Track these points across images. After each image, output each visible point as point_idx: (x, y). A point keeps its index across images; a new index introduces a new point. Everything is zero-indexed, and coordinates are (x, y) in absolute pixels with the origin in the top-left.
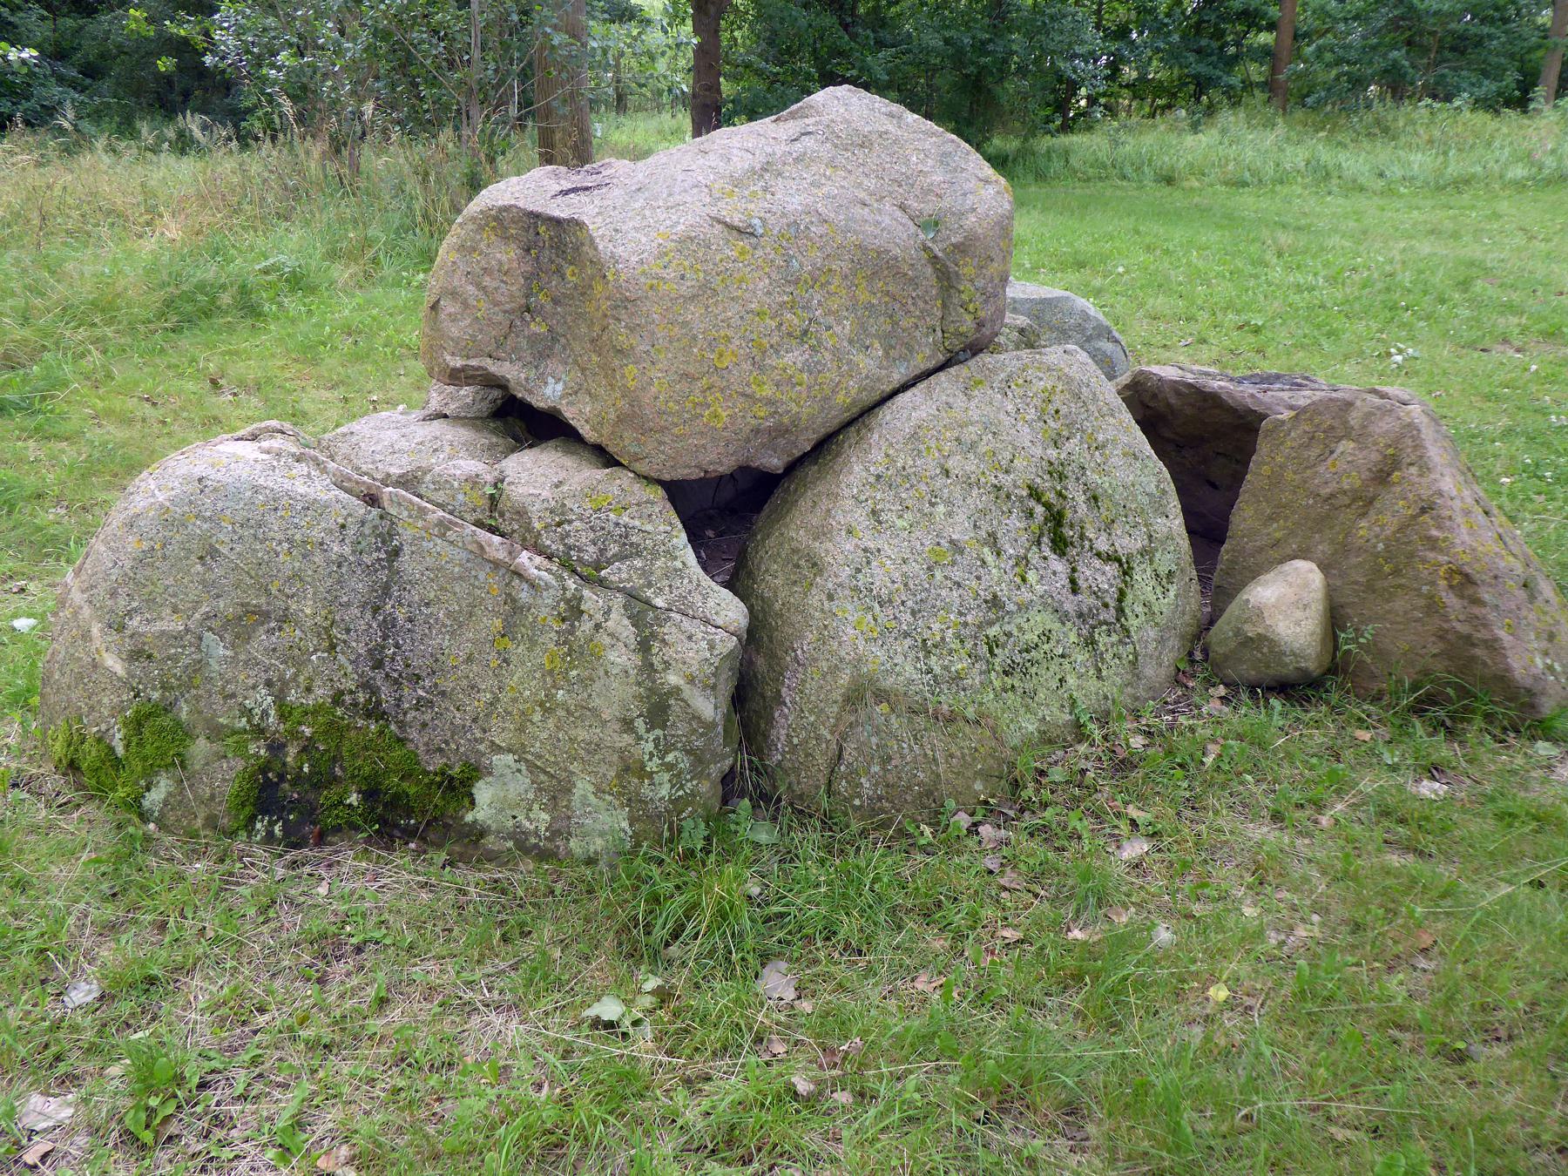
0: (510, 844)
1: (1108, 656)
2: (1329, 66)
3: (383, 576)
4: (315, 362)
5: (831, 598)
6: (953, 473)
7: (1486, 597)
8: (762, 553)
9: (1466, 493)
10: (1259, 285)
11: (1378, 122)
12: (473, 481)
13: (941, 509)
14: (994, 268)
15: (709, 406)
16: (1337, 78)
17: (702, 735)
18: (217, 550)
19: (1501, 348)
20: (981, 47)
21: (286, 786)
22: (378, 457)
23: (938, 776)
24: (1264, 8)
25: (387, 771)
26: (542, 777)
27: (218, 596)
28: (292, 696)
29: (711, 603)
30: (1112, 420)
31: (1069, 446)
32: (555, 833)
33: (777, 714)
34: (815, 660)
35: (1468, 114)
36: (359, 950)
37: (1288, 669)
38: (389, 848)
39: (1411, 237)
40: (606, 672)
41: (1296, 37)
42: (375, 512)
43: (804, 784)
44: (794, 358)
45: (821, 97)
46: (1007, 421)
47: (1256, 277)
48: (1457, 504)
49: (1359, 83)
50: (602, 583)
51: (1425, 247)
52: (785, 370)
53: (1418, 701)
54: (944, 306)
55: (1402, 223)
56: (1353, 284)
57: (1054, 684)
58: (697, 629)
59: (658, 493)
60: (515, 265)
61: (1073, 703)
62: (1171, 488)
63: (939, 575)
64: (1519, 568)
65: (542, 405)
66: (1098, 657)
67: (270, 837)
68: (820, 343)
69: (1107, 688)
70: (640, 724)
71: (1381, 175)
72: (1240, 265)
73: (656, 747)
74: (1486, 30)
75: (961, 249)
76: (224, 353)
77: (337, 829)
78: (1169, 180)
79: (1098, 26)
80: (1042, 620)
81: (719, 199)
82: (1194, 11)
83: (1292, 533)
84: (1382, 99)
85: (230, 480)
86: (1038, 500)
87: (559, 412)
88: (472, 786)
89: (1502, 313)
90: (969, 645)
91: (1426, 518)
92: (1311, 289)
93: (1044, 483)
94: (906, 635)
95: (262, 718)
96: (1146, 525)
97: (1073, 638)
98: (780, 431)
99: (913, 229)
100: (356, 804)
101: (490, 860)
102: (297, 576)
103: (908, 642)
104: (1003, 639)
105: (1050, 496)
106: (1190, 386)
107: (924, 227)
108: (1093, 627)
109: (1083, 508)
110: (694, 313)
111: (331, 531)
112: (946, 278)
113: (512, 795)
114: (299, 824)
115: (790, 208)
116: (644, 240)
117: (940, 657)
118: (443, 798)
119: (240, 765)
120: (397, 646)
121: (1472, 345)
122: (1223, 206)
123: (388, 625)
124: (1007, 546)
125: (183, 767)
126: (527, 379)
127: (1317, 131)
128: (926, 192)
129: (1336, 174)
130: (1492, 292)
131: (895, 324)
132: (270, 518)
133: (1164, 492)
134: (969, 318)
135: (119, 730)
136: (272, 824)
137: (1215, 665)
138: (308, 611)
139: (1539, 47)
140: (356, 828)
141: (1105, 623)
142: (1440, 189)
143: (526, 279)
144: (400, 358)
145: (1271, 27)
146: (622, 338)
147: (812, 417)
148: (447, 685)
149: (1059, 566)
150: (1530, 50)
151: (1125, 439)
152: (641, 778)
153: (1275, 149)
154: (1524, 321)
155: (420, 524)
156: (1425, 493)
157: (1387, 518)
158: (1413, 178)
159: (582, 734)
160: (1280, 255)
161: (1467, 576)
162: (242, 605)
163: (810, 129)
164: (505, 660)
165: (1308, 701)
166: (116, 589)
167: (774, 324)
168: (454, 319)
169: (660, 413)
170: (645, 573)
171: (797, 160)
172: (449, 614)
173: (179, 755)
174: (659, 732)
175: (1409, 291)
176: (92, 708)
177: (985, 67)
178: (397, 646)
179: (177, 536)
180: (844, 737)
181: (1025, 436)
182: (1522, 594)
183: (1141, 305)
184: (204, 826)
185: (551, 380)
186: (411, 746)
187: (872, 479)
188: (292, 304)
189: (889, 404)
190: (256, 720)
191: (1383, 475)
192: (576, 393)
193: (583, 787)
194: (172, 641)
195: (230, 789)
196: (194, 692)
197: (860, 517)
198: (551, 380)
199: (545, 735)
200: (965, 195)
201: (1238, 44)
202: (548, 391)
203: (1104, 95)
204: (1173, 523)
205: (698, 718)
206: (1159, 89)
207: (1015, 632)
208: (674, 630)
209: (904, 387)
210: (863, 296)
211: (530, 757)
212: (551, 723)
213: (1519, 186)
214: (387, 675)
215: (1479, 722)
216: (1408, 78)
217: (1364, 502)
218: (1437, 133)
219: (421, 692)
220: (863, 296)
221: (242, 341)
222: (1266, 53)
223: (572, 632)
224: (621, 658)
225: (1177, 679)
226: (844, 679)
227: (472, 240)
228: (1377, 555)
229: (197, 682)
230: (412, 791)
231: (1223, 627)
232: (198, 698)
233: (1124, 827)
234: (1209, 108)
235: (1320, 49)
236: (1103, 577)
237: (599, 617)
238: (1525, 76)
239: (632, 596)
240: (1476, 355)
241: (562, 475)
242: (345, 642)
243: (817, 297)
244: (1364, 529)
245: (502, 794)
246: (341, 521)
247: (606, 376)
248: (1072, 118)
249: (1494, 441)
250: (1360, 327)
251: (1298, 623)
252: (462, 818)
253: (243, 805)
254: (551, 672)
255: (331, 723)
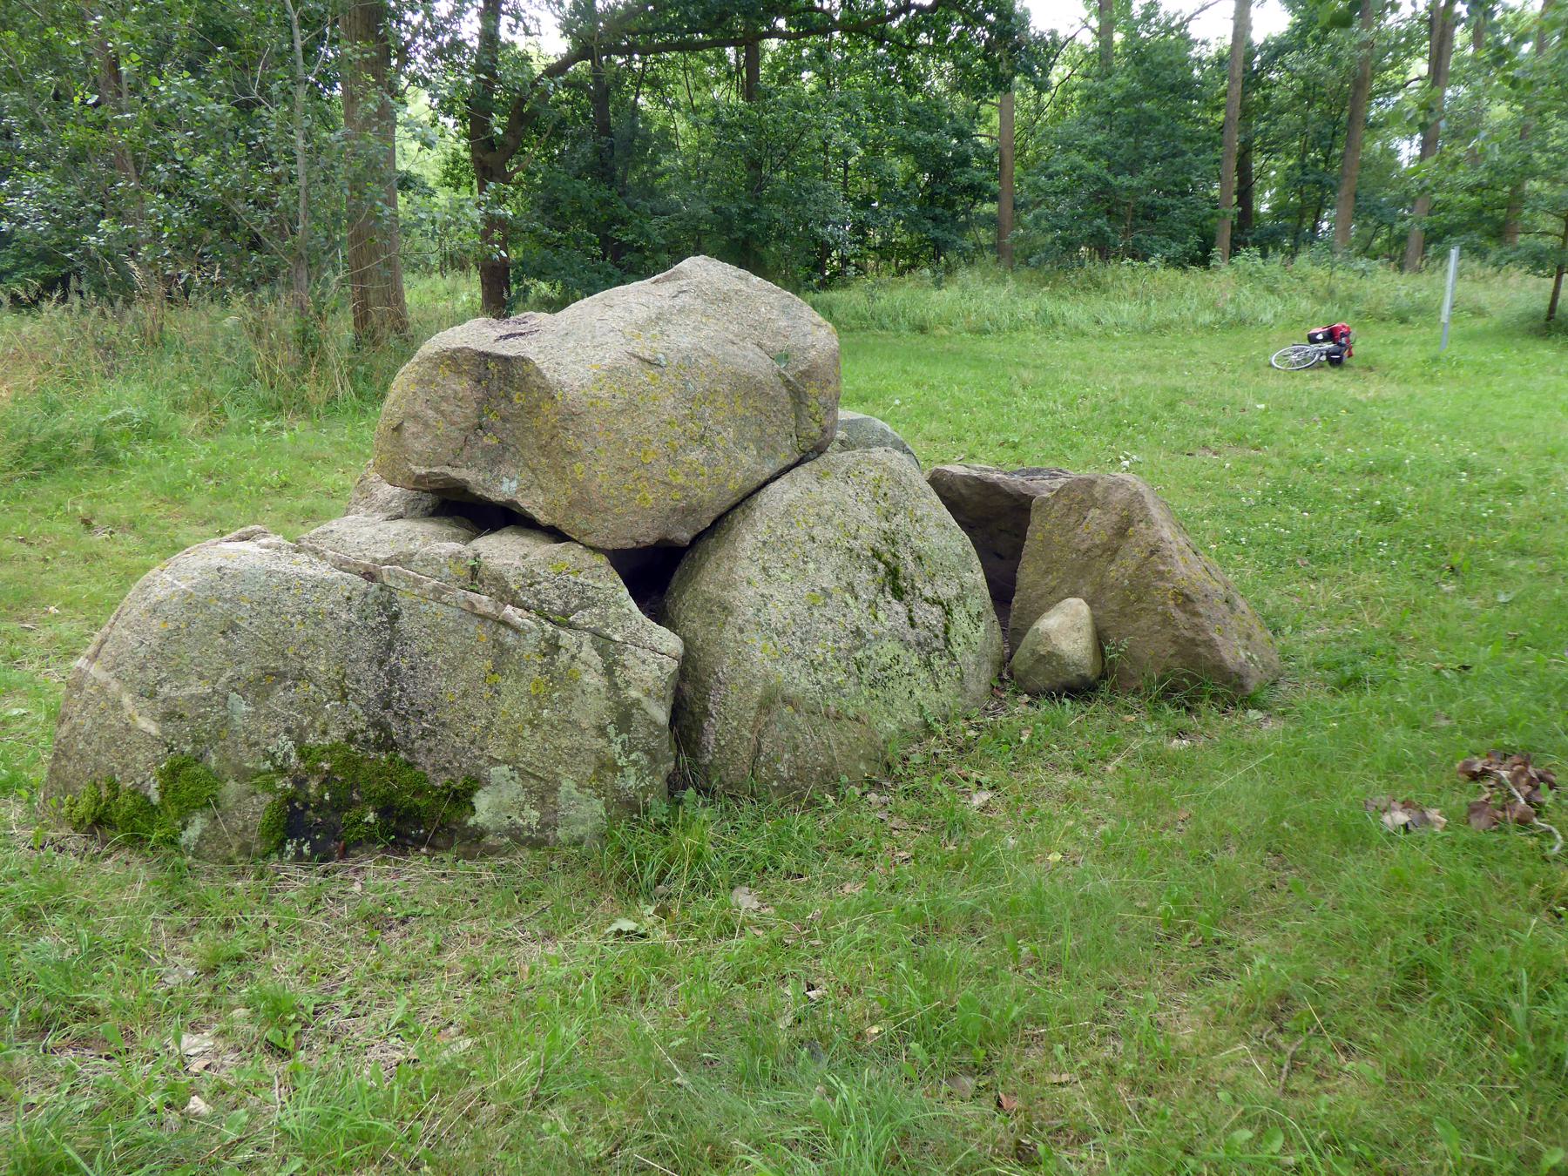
0: (507, 839)
1: (942, 675)
2: (1046, 231)
3: (386, 635)
4: (184, 502)
5: (741, 631)
6: (818, 539)
7: (1202, 610)
8: (680, 605)
9: (1180, 539)
10: (1012, 411)
11: (1090, 278)
12: (457, 557)
13: (811, 566)
14: (831, 388)
15: (639, 492)
16: (1053, 243)
17: (657, 737)
18: (237, 625)
19: (1202, 452)
20: (747, 216)
21: (310, 813)
22: (363, 547)
23: (834, 758)
24: (987, 182)
25: (400, 790)
26: (532, 781)
27: (240, 663)
28: (311, 739)
29: (655, 637)
30: (925, 501)
31: (897, 520)
32: (545, 825)
33: (705, 725)
34: (734, 679)
35: (1162, 271)
36: (403, 922)
37: (1072, 676)
38: (404, 853)
39: (1126, 372)
40: (583, 692)
41: (1015, 207)
42: (375, 586)
43: (733, 775)
44: (696, 455)
45: (686, 264)
46: (851, 502)
47: (1008, 405)
48: (1175, 546)
49: (1070, 245)
50: (571, 626)
51: (1139, 379)
52: (691, 464)
53: (1165, 690)
54: (797, 416)
55: (1119, 360)
56: (1085, 408)
57: (906, 695)
58: (649, 656)
59: (602, 560)
60: (468, 393)
61: (921, 708)
62: (973, 550)
63: (816, 614)
64: (1221, 590)
65: (500, 499)
66: (935, 675)
67: (299, 855)
68: (714, 445)
69: (943, 698)
70: (611, 730)
71: (1098, 322)
72: (994, 395)
73: (623, 748)
74: (1169, 201)
75: (807, 375)
76: (90, 497)
77: (358, 843)
78: (922, 329)
79: (847, 198)
80: (891, 648)
81: (631, 340)
82: (927, 184)
83: (1063, 581)
84: (1092, 259)
85: (246, 568)
86: (880, 559)
87: (515, 503)
88: (471, 796)
89: (1201, 426)
90: (844, 664)
91: (1154, 558)
92: (1053, 413)
93: (883, 547)
94: (799, 657)
95: (284, 760)
96: (958, 578)
97: (915, 661)
98: (689, 511)
99: (770, 361)
100: (372, 821)
101: (492, 854)
102: (311, 641)
103: (800, 662)
104: (866, 661)
105: (887, 556)
106: (976, 478)
107: (777, 359)
108: (929, 653)
109: (911, 566)
110: (623, 423)
111: (339, 603)
112: (798, 397)
113: (506, 800)
114: (324, 842)
115: (682, 345)
116: (582, 370)
117: (825, 672)
118: (449, 807)
119: (269, 798)
120: (402, 689)
121: (1180, 451)
122: (971, 350)
123: (394, 674)
124: (861, 593)
125: (217, 806)
126: (484, 480)
127: (1041, 286)
128: (777, 333)
129: (1061, 322)
130: (1191, 410)
131: (763, 431)
132: (285, 596)
133: (968, 553)
134: (815, 425)
135: (155, 781)
136: (300, 845)
137: (1020, 680)
138: (322, 668)
139: (1212, 215)
140: (374, 841)
141: (938, 650)
142: (1147, 332)
143: (478, 403)
144: (265, 495)
145: (994, 198)
146: (571, 442)
147: (712, 500)
148: (447, 718)
149: (898, 607)
150: (1205, 219)
151: (936, 514)
152: (614, 773)
153: (1009, 301)
154: (1217, 431)
155: (416, 592)
156: (1152, 541)
157: (1128, 562)
158: (1124, 324)
159: (565, 742)
160: (1024, 388)
161: (1187, 596)
162: (262, 668)
163: (685, 288)
164: (496, 692)
165: (1089, 700)
166: (144, 664)
167: (681, 431)
168: (416, 436)
169: (604, 497)
170: (601, 617)
171: (680, 311)
172: (445, 661)
173: (213, 796)
174: (625, 736)
175: (1129, 412)
176: (127, 766)
177: (751, 233)
178: (402, 689)
179: (201, 616)
180: (761, 735)
181: (865, 513)
182: (1225, 608)
183: (919, 430)
184: (239, 854)
185: (505, 479)
186: (420, 769)
187: (760, 545)
188: (148, 451)
189: (764, 490)
190: (279, 762)
191: (1122, 530)
192: (529, 488)
193: (567, 785)
194: (202, 702)
195: (259, 820)
196: (221, 743)
197: (754, 572)
198: (505, 479)
199: (533, 747)
200: (805, 335)
201: (966, 212)
202: (505, 488)
203: (855, 256)
204: (976, 576)
205: (653, 722)
206: (903, 251)
207: (874, 656)
208: (631, 657)
209: (773, 479)
210: (740, 411)
211: (522, 766)
212: (538, 737)
213: (1209, 329)
214: (396, 714)
215: (1207, 700)
216: (1111, 241)
217: (1111, 551)
218: (1139, 287)
219: (425, 725)
220: (740, 411)
221: (102, 484)
222: (991, 221)
223: (552, 664)
224: (593, 679)
225: (993, 691)
226: (758, 690)
227: (429, 375)
228: (1124, 589)
229: (224, 734)
230: (423, 803)
231: (1023, 652)
232: (225, 748)
233: (973, 786)
234: (947, 267)
235: (1037, 219)
236: (934, 615)
237: (574, 650)
238: (1205, 239)
239: (596, 634)
240: (1184, 458)
241: (526, 550)
242: (356, 690)
243: (708, 411)
244: (1113, 572)
245: (497, 801)
246: (346, 594)
247: (556, 473)
248: (829, 277)
249: (1202, 520)
250: (1095, 440)
251: (1075, 642)
252: (466, 822)
253: (274, 831)
254: (536, 697)
255: (346, 758)
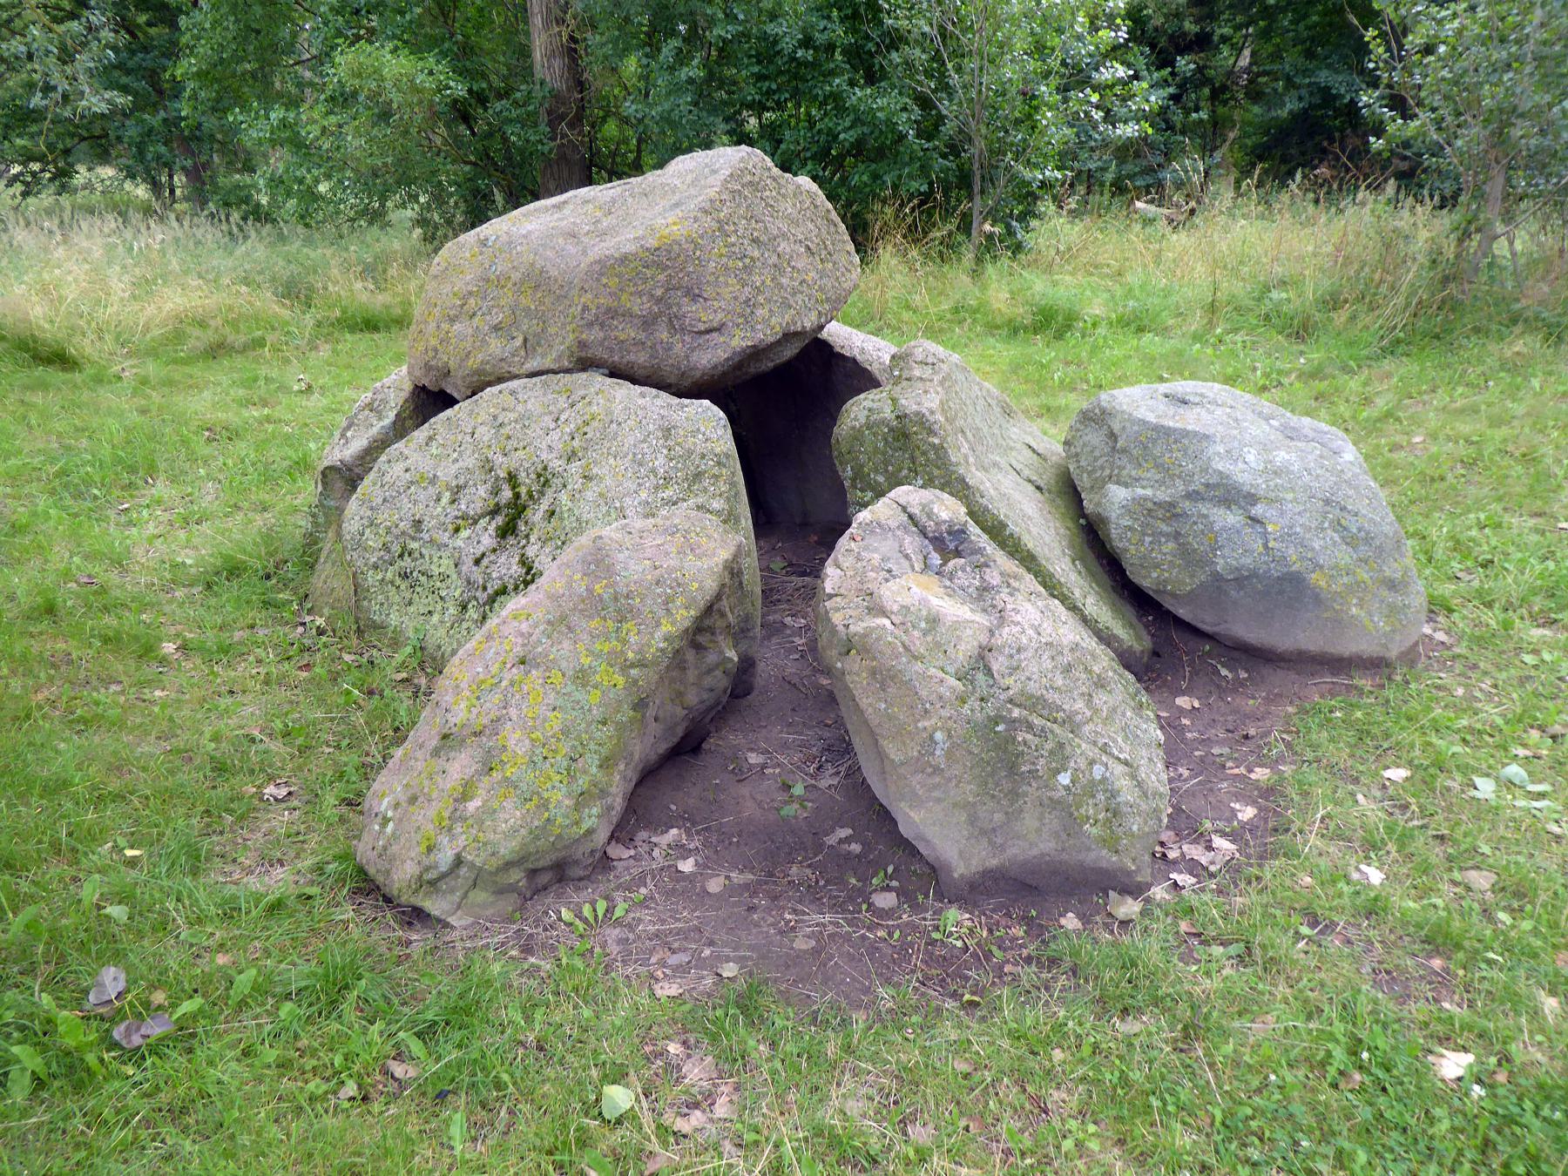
30: (612, 461)
104: (417, 555)
109: (540, 514)
